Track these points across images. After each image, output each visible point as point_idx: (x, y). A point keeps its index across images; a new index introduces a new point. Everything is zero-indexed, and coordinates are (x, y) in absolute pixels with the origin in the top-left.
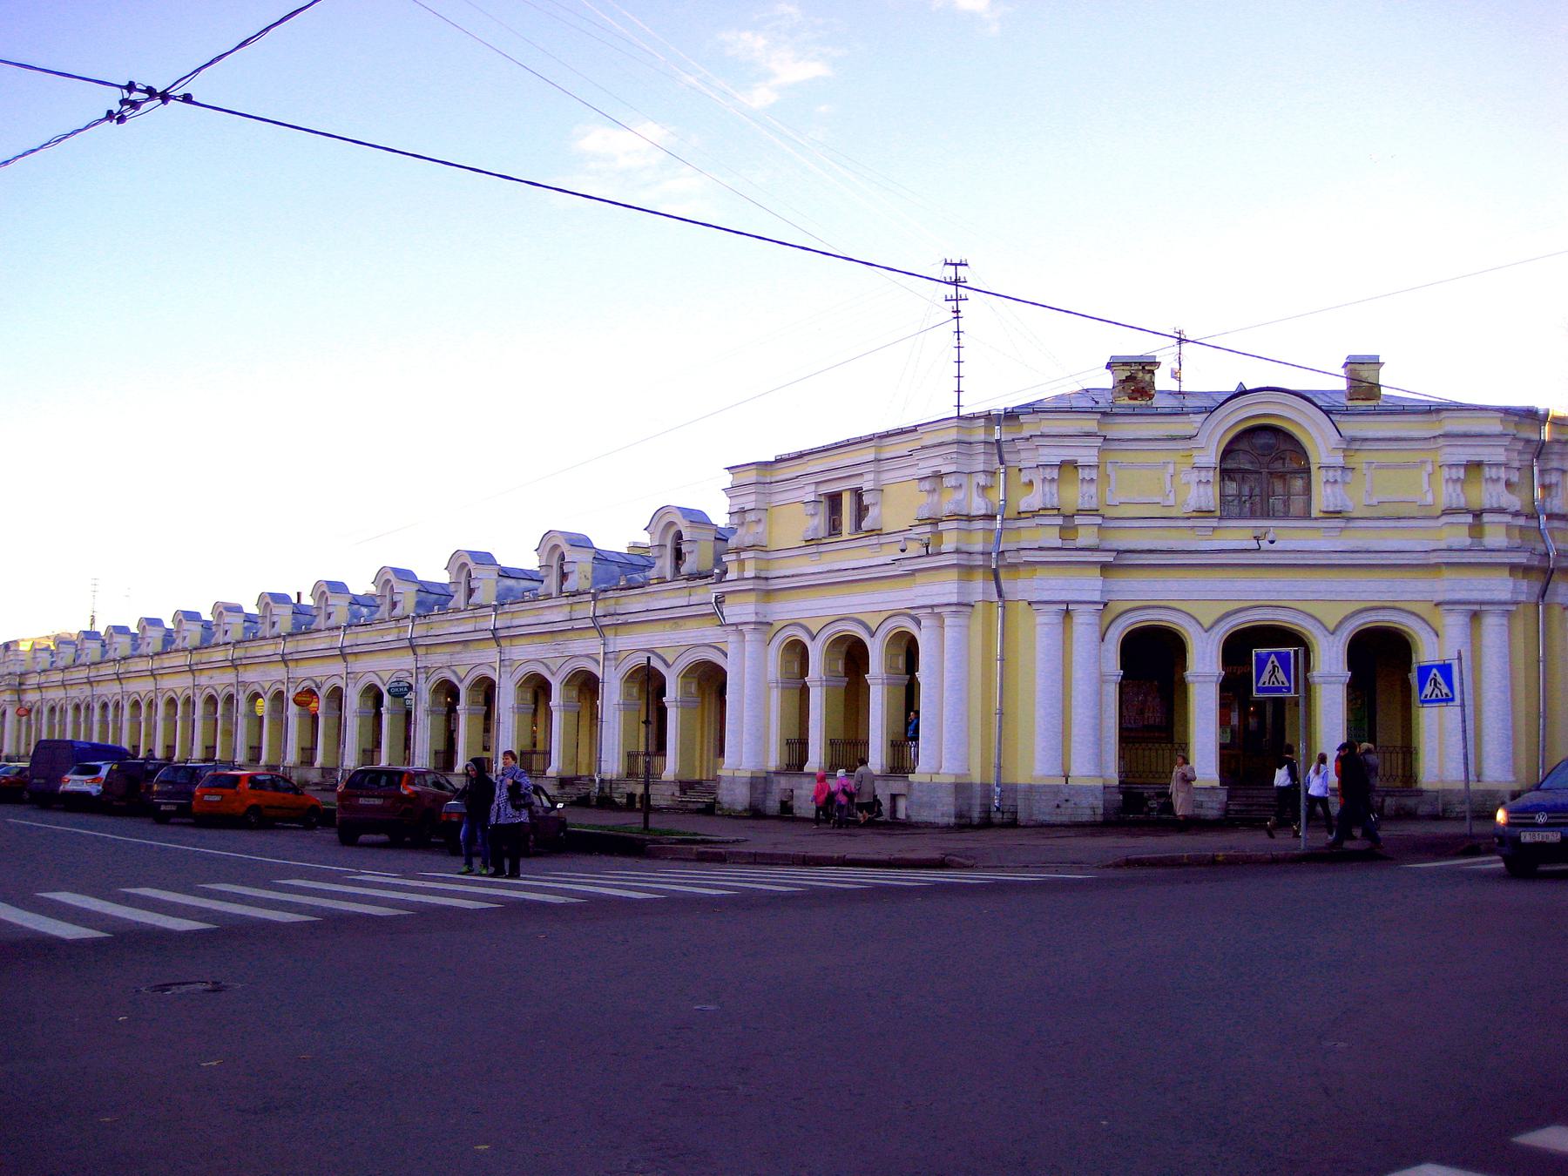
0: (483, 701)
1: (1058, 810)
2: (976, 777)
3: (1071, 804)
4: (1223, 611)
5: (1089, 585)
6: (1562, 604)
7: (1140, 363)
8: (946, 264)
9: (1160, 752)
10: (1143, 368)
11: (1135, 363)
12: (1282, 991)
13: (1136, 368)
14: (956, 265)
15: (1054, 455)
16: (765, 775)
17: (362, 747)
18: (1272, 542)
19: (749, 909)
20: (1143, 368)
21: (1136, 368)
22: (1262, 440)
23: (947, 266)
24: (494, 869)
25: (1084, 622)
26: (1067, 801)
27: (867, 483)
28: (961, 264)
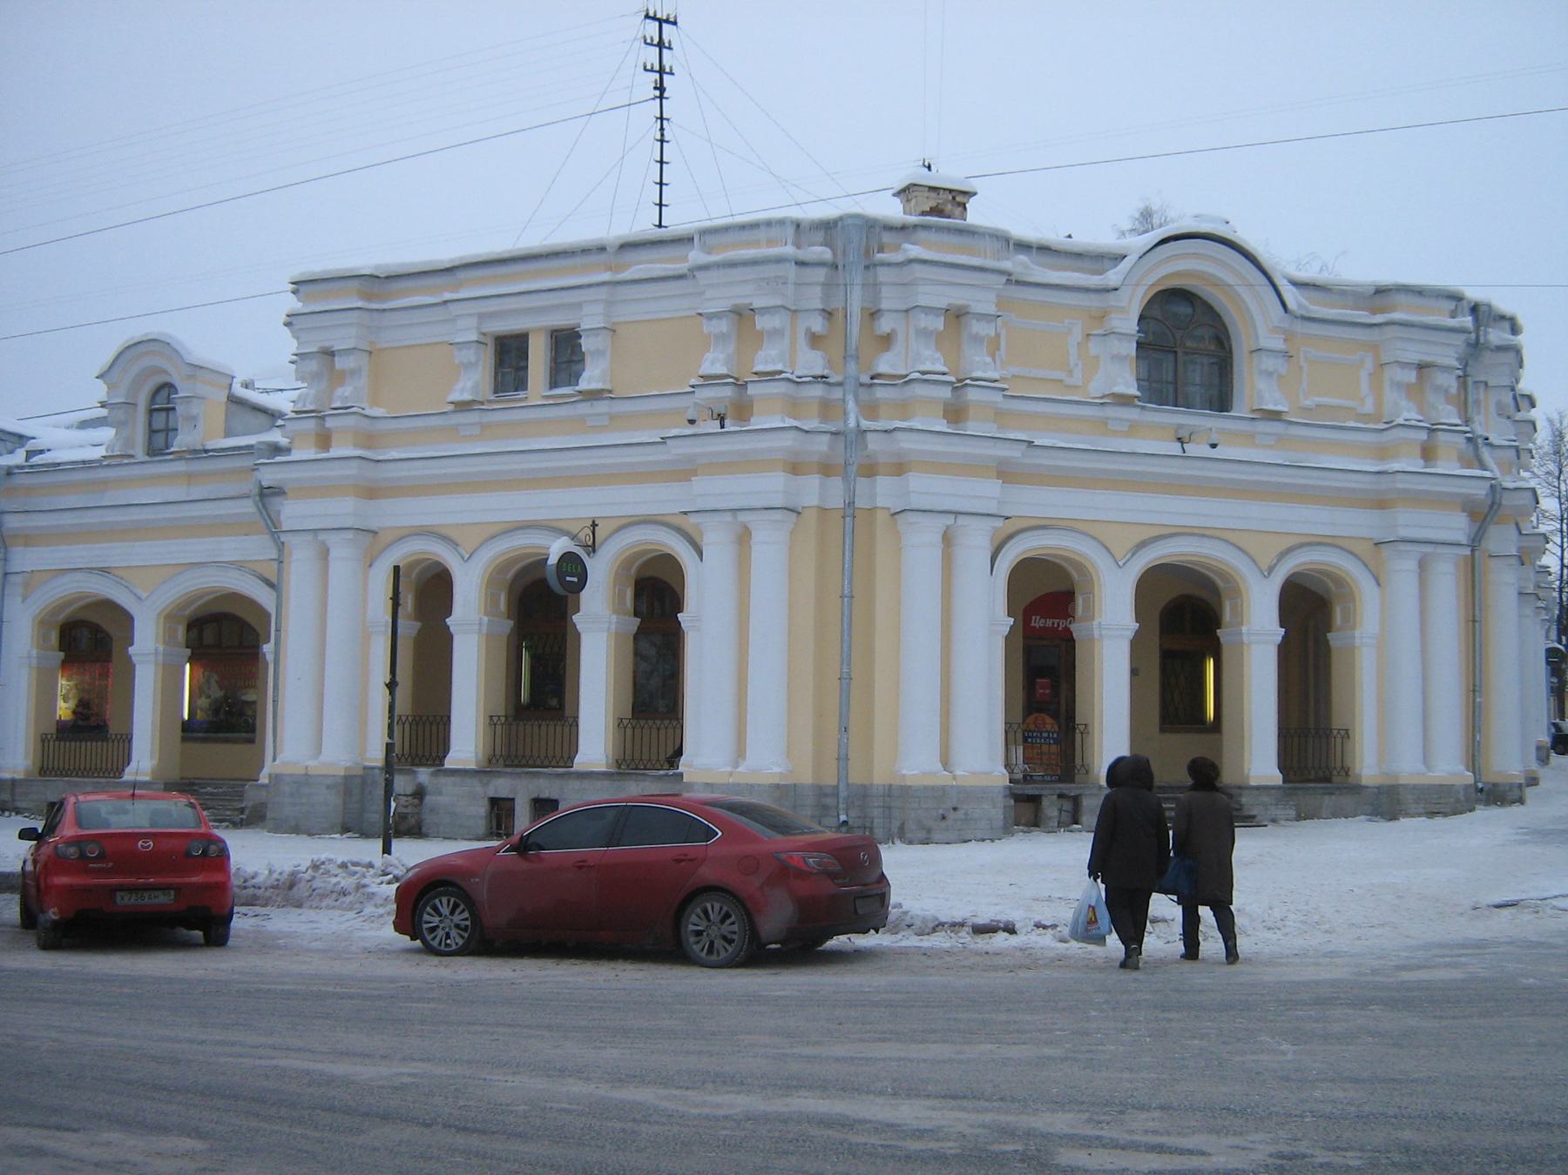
0: (58, 644)
1: (943, 824)
2: (806, 777)
3: (960, 814)
4: (1284, 547)
5: (986, 492)
6: (1371, 539)
7: (951, 191)
8: (647, 16)
9: (662, 732)
10: (954, 198)
11: (944, 189)
12: (1119, 1092)
13: (945, 197)
14: (661, 21)
15: (1414, 354)
16: (360, 772)
17: (616, 717)
18: (1214, 446)
19: (974, 964)
20: (954, 198)
21: (945, 197)
22: (1184, 309)
23: (647, 21)
24: (1156, 898)
25: (976, 541)
26: (955, 809)
27: (589, 319)
28: (667, 21)
